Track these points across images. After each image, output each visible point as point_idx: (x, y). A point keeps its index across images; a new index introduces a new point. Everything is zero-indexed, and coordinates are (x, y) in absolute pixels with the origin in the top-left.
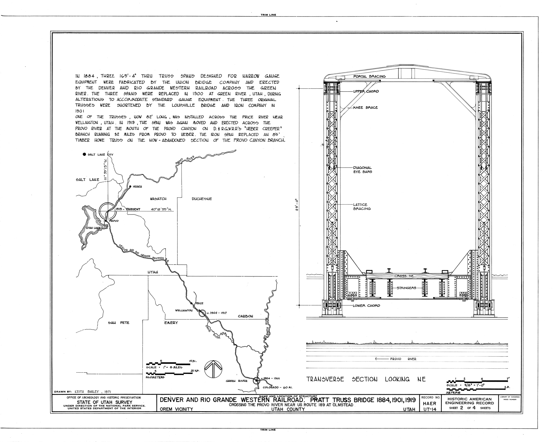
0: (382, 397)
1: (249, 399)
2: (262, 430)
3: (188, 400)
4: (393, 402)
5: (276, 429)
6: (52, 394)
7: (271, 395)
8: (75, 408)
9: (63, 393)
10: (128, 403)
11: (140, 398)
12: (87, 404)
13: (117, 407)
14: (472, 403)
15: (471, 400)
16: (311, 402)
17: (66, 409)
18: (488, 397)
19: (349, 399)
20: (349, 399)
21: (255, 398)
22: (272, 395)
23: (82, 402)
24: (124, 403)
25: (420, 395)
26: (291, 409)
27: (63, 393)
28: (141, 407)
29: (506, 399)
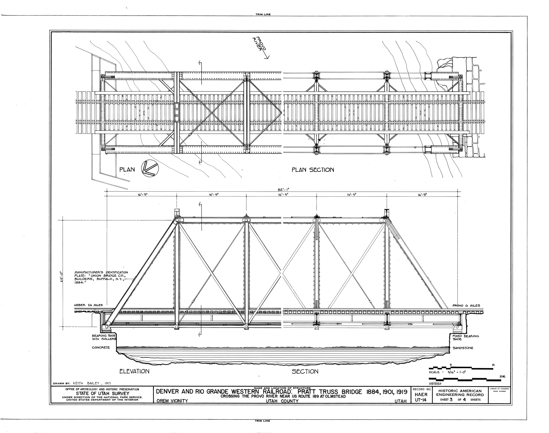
0: (372, 388)
1: (240, 391)
5: (270, 420)
6: (51, 386)
7: (265, 387)
8: (73, 400)
9: (62, 385)
10: (125, 394)
11: (138, 389)
12: (86, 395)
13: (115, 398)
15: (462, 391)
17: (64, 400)
18: (478, 389)
19: (336, 391)
20: (336, 391)
21: (246, 390)
22: (267, 387)
24: (121, 394)
25: (411, 387)
26: (285, 401)
27: (62, 385)
28: (138, 398)
29: (495, 391)
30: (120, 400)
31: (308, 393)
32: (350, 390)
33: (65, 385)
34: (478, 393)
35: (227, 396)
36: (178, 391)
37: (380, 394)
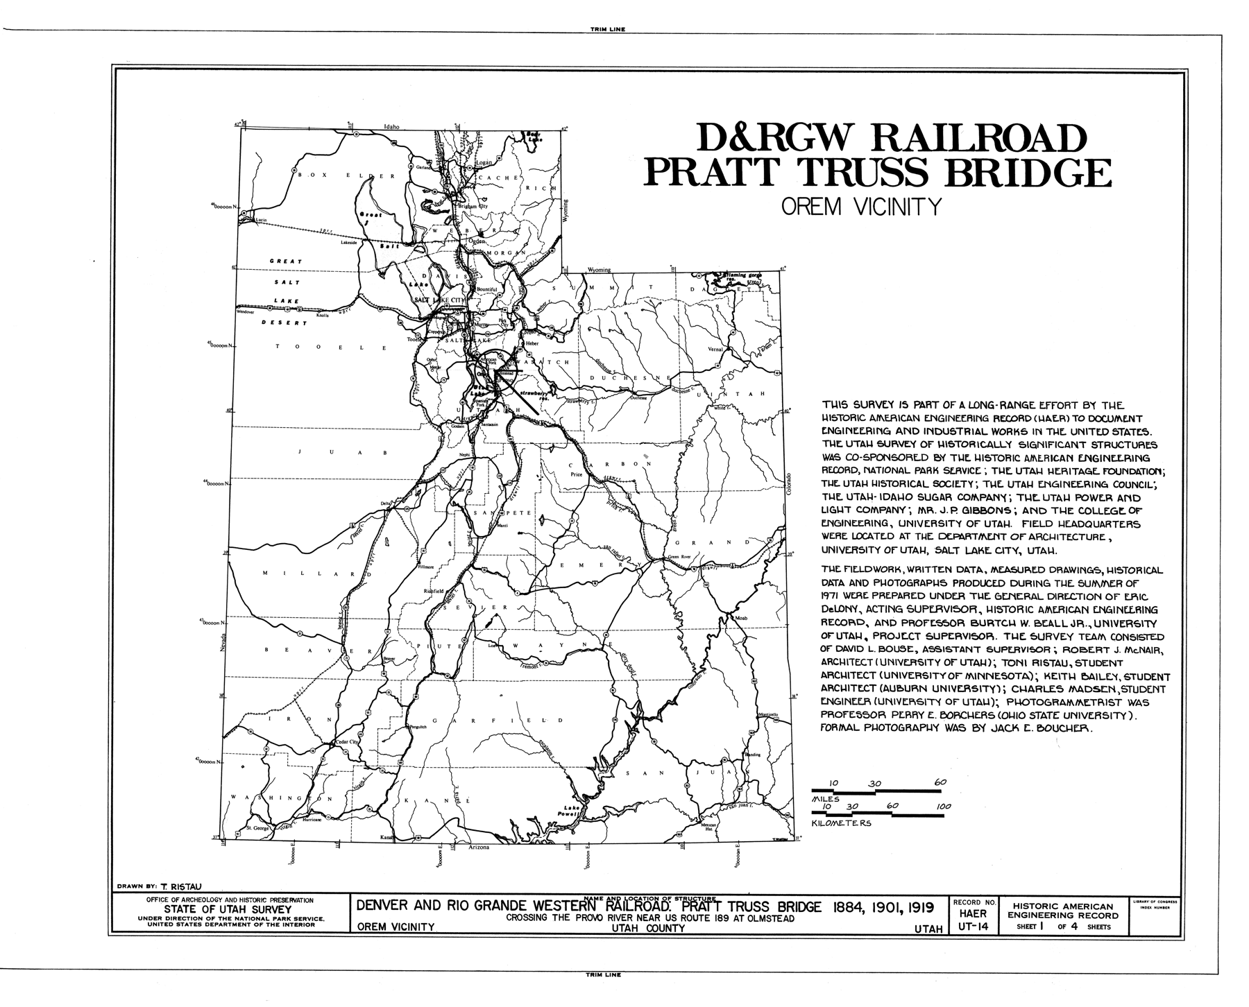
0: (845, 900)
1: (552, 903)
2: (590, 975)
3: (418, 906)
5: (622, 974)
6: (112, 892)
7: (610, 897)
8: (163, 924)
10: (281, 911)
11: (311, 900)
12: (189, 914)
16: (683, 910)
17: (143, 926)
18: (1106, 901)
19: (765, 904)
21: (566, 902)
22: (614, 896)
24: (272, 910)
25: (949, 896)
26: (655, 928)
28: (314, 922)
29: (1146, 908)
33: (145, 889)
36: (405, 905)
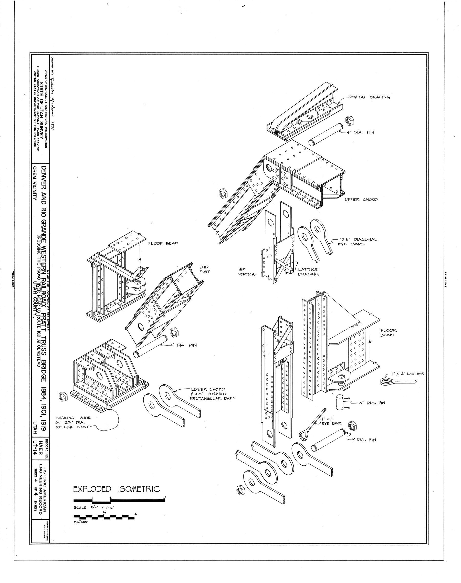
0: (47, 392)
2: (13, 273)
3: (43, 194)
4: (42, 405)
5: (13, 288)
6: (50, 54)
7: (49, 282)
8: (35, 78)
9: (51, 66)
10: (41, 134)
12: (40, 93)
13: (37, 122)
14: (41, 492)
15: (44, 491)
17: (34, 69)
18: (47, 509)
19: (45, 353)
20: (45, 353)
21: (46, 260)
22: (49, 284)
23: (42, 112)
24: (41, 130)
25: (49, 437)
27: (51, 66)
28: (37, 147)
29: (45, 527)
30: (35, 127)
31: (43, 323)
32: (46, 369)
33: (51, 69)
34: (43, 508)
35: (39, 241)
37: (42, 401)
